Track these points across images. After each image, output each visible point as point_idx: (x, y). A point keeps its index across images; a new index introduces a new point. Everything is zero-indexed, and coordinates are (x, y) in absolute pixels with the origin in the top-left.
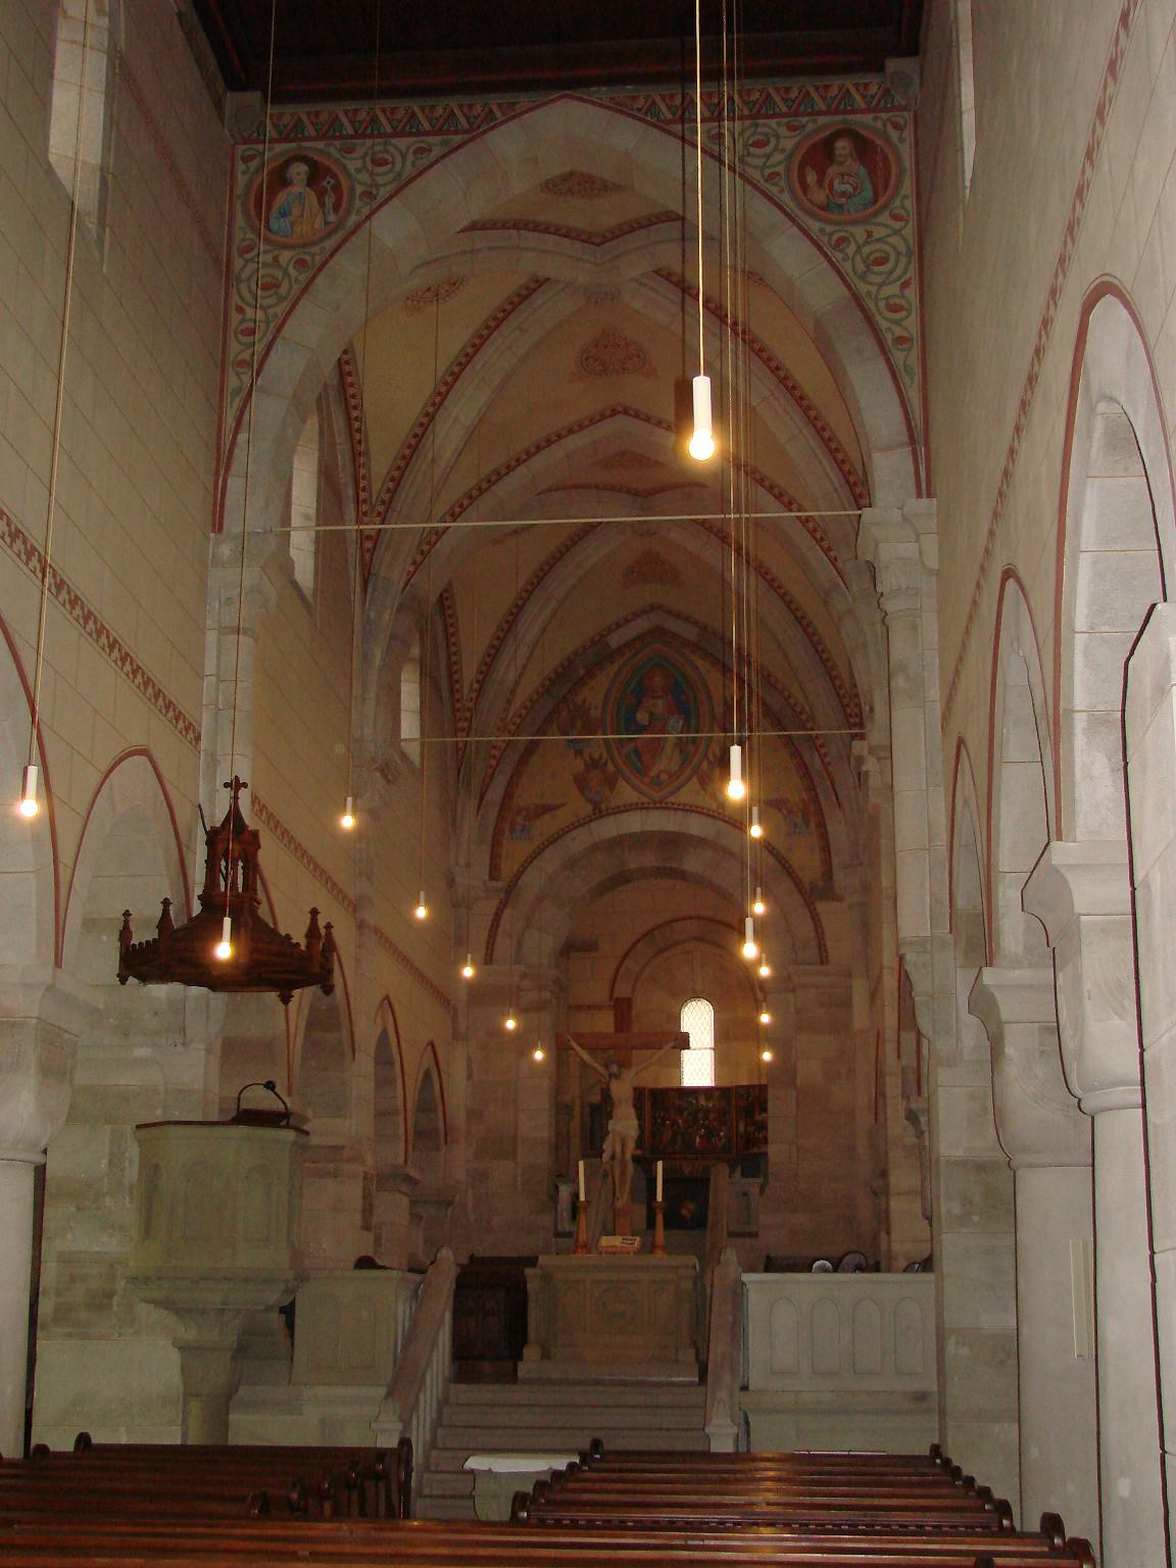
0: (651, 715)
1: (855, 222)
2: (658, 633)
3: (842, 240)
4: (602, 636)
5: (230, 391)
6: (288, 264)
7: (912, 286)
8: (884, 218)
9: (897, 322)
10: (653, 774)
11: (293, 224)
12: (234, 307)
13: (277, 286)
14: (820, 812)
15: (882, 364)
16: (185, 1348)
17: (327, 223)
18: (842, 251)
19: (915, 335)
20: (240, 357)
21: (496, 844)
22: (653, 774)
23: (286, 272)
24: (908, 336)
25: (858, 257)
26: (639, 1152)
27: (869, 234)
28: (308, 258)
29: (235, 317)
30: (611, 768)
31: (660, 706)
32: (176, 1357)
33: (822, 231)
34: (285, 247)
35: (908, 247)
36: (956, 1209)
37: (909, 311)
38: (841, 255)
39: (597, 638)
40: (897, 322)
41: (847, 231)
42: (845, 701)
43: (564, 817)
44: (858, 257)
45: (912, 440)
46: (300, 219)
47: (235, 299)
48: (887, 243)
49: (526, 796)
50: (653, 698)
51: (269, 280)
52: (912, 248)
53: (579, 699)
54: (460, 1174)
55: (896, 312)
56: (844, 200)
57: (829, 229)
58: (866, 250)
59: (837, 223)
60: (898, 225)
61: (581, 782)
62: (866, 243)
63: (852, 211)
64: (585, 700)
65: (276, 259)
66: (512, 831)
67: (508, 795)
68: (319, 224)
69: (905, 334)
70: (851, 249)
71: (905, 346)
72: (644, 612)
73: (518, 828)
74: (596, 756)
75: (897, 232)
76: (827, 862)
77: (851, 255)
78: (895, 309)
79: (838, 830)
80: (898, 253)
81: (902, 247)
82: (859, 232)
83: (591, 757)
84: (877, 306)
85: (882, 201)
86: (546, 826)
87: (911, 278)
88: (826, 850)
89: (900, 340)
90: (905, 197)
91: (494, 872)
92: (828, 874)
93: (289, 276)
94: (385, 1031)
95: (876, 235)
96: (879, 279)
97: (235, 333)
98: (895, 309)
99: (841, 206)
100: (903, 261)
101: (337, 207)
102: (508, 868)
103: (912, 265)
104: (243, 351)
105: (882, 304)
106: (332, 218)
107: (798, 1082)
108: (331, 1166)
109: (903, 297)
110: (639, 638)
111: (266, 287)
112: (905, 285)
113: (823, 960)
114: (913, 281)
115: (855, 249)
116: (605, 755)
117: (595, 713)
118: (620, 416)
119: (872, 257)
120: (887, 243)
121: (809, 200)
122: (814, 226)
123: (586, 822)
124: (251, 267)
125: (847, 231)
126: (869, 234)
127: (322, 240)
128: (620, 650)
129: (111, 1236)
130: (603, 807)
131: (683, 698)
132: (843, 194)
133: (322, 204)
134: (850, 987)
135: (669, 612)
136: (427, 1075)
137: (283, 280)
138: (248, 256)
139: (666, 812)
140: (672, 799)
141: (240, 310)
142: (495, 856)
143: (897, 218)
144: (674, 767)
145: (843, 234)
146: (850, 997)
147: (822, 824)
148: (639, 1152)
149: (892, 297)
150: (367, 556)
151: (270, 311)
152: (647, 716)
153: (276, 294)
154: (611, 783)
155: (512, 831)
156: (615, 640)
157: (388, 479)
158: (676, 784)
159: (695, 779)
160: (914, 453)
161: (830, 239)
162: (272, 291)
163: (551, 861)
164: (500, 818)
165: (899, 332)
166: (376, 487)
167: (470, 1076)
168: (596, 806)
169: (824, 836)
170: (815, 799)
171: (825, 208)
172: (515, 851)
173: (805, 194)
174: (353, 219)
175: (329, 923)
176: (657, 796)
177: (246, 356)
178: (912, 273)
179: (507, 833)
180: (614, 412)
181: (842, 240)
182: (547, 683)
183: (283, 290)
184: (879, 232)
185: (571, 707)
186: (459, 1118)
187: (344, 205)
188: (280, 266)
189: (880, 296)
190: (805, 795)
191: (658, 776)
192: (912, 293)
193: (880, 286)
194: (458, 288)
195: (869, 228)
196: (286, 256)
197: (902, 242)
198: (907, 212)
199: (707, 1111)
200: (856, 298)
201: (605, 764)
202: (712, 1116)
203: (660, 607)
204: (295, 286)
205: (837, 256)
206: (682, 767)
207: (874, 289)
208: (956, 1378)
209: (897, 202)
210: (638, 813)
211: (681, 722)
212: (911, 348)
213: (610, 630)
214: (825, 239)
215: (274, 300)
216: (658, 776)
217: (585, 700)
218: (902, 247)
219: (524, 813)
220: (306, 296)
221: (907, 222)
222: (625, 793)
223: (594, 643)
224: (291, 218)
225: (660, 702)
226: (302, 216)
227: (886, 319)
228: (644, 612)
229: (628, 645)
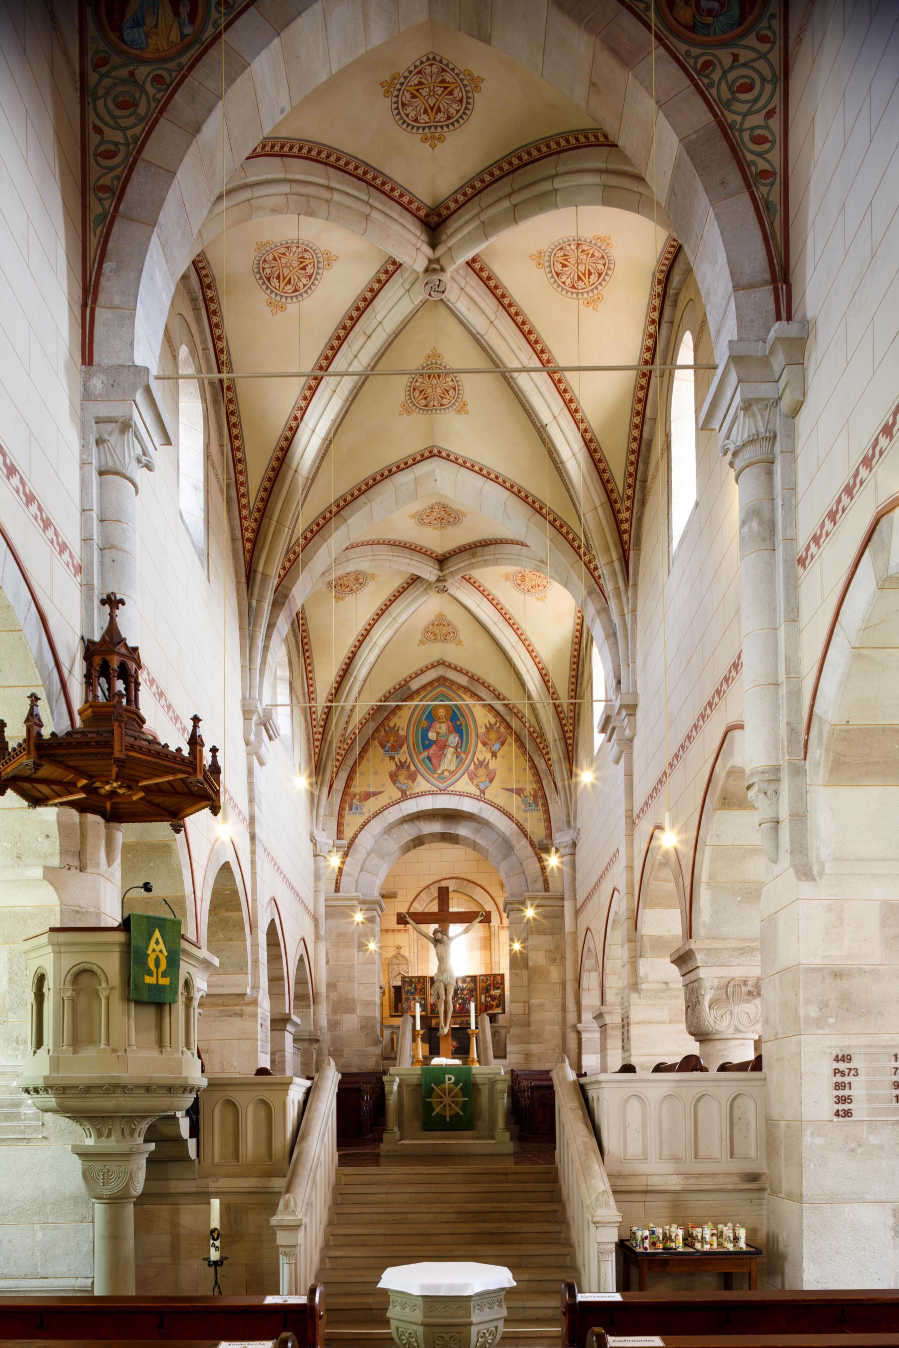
0: (438, 734)
1: (724, 44)
2: (442, 680)
3: (707, 64)
4: (407, 682)
5: (92, 218)
6: (145, 81)
7: (777, 116)
8: (751, 40)
9: (760, 155)
10: (439, 772)
11: (147, 35)
12: (91, 126)
13: (135, 105)
14: (544, 797)
15: (746, 197)
16: (84, 1155)
17: (183, 36)
18: (707, 77)
19: (778, 171)
20: (101, 182)
21: (340, 816)
22: (439, 772)
23: (144, 91)
24: (770, 169)
25: (723, 84)
26: (424, 1013)
27: (736, 58)
28: (165, 74)
29: (94, 138)
30: (412, 768)
31: (443, 728)
32: (77, 1164)
33: (688, 54)
34: (144, 61)
35: (774, 75)
36: (814, 1012)
37: (773, 143)
38: (706, 81)
39: (403, 683)
40: (760, 155)
41: (712, 55)
42: (564, 722)
43: (383, 800)
44: (723, 84)
45: (774, 280)
46: (154, 30)
47: (92, 118)
48: (752, 68)
49: (358, 787)
50: (440, 723)
51: (127, 98)
52: (778, 74)
53: (392, 724)
54: (324, 1022)
55: (759, 144)
56: (711, 19)
57: (695, 51)
58: (731, 76)
59: (702, 45)
60: (764, 47)
61: (394, 777)
62: (732, 67)
63: (718, 32)
64: (395, 725)
65: (132, 74)
66: (351, 809)
67: (347, 785)
68: (174, 36)
69: (769, 168)
70: (716, 76)
71: (768, 181)
72: (433, 666)
73: (354, 806)
74: (403, 760)
75: (763, 56)
76: (549, 828)
77: (716, 80)
78: (759, 140)
79: (556, 808)
80: (763, 79)
81: (768, 74)
82: (725, 55)
83: (400, 761)
84: (741, 137)
85: (750, 19)
86: (372, 805)
87: (775, 108)
88: (548, 820)
89: (764, 174)
90: (773, 16)
91: (340, 834)
92: (550, 836)
93: (147, 94)
94: (273, 920)
95: (742, 60)
96: (744, 108)
97: (95, 155)
98: (759, 140)
99: (707, 26)
100: (768, 87)
101: (192, 17)
102: (349, 832)
103: (777, 91)
104: (104, 174)
105: (746, 136)
106: (188, 30)
107: (530, 964)
108: (237, 1008)
109: (767, 127)
110: (430, 683)
111: (122, 106)
112: (770, 114)
113: (547, 889)
114: (777, 110)
115: (720, 74)
116: (409, 760)
117: (402, 733)
118: (435, 459)
119: (738, 84)
120: (752, 68)
121: (675, 19)
122: (681, 47)
123: (398, 802)
124: (107, 82)
125: (712, 55)
126: (736, 58)
127: (179, 54)
128: (418, 692)
129: (15, 1050)
130: (408, 793)
131: (458, 723)
132: (710, 13)
133: (177, 14)
134: (563, 906)
135: (449, 666)
136: (301, 960)
137: (140, 98)
138: (103, 70)
139: (448, 796)
140: (451, 788)
141: (98, 130)
142: (340, 825)
143: (763, 39)
144: (453, 768)
145: (710, 58)
146: (563, 912)
147: (546, 805)
148: (424, 1013)
149: (758, 127)
150: (248, 555)
151: (130, 133)
152: (435, 734)
153: (134, 113)
154: (412, 778)
155: (351, 809)
156: (415, 685)
157: (262, 489)
158: (454, 778)
159: (466, 775)
160: (776, 291)
161: (695, 63)
162: (131, 110)
163: (376, 827)
164: (343, 801)
165: (762, 165)
166: (253, 495)
167: (327, 963)
168: (403, 792)
169: (547, 812)
170: (542, 788)
171: (692, 29)
172: (353, 822)
173: (671, 12)
174: (210, 31)
175: (214, 747)
176: (442, 786)
177: (106, 181)
178: (777, 101)
179: (347, 809)
180: (432, 455)
181: (707, 64)
182: (371, 712)
183: (142, 109)
184: (745, 56)
185: (387, 728)
186: (323, 989)
187: (200, 12)
188: (136, 82)
189: (745, 127)
190: (535, 786)
191: (443, 773)
192: (775, 123)
193: (745, 115)
194: (316, 279)
195: (736, 51)
196: (142, 71)
197: (768, 68)
198: (774, 33)
199: (463, 989)
200: (722, 125)
201: (409, 766)
202: (465, 992)
203: (444, 663)
204: (153, 105)
205: (703, 82)
206: (458, 768)
207: (738, 118)
208: (812, 1165)
209: (764, 23)
210: (430, 797)
211: (457, 738)
212: (772, 184)
213: (412, 678)
214: (692, 61)
215: (132, 120)
216: (443, 773)
217: (395, 725)
218: (768, 74)
219: (358, 797)
220: (165, 114)
221: (774, 43)
222: (421, 784)
223: (401, 686)
224: (146, 29)
225: (444, 726)
226: (156, 27)
227: (751, 152)
228: (433, 666)
229: (423, 688)
